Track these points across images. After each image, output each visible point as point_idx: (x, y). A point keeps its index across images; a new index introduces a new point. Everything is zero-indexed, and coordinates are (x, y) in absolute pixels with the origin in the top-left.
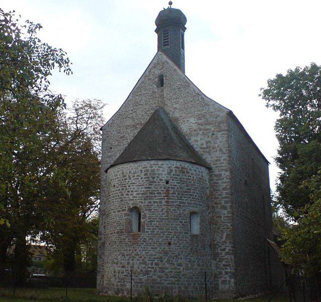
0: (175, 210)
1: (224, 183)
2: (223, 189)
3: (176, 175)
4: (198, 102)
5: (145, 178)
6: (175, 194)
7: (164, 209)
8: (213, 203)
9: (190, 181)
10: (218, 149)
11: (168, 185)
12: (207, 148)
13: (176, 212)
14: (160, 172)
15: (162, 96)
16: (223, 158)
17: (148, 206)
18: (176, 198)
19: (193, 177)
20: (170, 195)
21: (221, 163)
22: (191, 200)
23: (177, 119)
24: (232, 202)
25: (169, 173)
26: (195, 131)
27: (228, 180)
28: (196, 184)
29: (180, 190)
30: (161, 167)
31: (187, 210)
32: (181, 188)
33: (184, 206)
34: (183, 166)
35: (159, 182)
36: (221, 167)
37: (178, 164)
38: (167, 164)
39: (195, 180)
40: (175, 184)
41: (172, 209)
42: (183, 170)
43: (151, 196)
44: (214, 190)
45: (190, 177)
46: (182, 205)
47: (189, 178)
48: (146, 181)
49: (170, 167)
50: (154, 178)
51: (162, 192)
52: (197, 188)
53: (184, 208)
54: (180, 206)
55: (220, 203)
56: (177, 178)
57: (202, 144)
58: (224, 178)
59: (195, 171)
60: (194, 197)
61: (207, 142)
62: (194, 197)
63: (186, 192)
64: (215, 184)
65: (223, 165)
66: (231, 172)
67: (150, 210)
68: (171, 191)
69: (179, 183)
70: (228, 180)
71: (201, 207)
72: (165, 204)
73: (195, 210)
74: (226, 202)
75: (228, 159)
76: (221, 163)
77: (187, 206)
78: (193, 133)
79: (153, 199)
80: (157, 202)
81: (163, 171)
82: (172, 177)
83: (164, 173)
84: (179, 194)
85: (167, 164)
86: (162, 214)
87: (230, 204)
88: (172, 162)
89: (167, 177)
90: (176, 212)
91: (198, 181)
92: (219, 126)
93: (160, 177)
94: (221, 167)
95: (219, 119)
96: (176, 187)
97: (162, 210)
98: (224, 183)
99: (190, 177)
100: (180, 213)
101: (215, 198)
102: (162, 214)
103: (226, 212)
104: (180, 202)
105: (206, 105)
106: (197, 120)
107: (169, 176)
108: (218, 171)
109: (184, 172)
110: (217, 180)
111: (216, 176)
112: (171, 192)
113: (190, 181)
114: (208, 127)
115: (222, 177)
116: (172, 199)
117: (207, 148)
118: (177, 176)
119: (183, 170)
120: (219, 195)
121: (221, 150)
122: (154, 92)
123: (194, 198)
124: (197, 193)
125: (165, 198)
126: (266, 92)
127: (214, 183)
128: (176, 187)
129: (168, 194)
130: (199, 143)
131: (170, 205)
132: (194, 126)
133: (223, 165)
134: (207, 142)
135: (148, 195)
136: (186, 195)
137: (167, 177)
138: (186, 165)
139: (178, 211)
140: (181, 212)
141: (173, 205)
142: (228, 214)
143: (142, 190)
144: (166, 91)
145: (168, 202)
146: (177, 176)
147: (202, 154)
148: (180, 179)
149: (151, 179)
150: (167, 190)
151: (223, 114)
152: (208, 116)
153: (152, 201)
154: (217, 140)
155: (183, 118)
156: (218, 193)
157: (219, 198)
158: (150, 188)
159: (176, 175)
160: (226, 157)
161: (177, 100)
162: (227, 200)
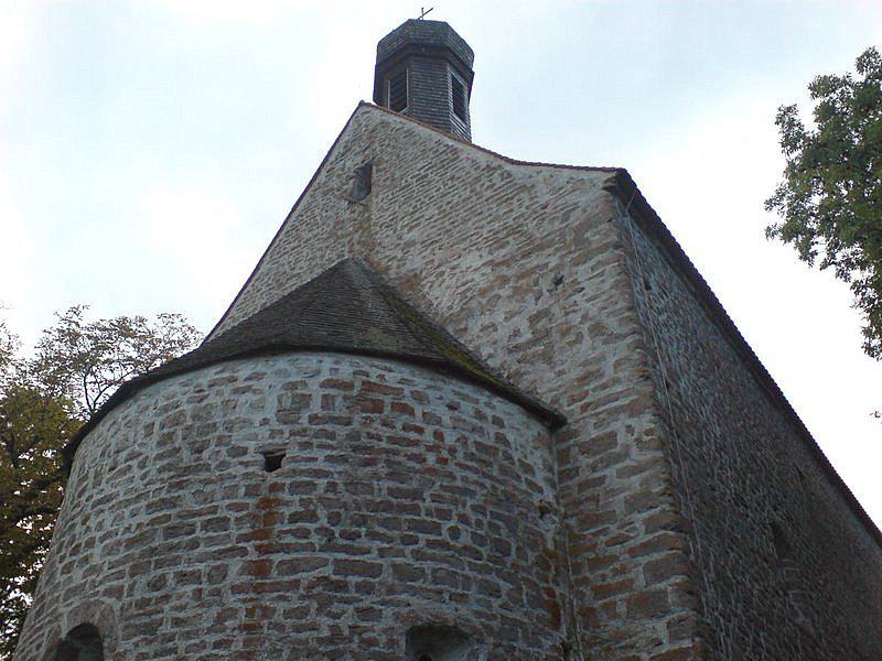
0: (304, 612)
1: (634, 471)
2: (633, 505)
3: (325, 420)
4: (489, 193)
5: (160, 457)
6: (313, 517)
7: (233, 613)
8: (587, 590)
9: (414, 450)
10: (585, 328)
11: (272, 477)
12: (534, 342)
13: (314, 627)
14: (242, 412)
15: (364, 225)
16: (612, 361)
17: (146, 602)
18: (315, 539)
19: (438, 436)
20: (278, 527)
21: (604, 387)
22: (419, 556)
23: (413, 280)
24: (693, 571)
25: (286, 415)
26: (483, 292)
27: (649, 455)
28: (459, 473)
29: (347, 497)
30: (244, 391)
31: (388, 611)
32: (352, 485)
33: (366, 589)
34: (373, 379)
35: (223, 465)
36: (609, 400)
37: (346, 368)
38: (279, 373)
39: (452, 451)
40: (321, 465)
41: (281, 606)
42: (372, 396)
43: (171, 548)
44: (588, 521)
45: (420, 430)
46: (353, 579)
47: (413, 436)
48: (160, 471)
49: (293, 386)
50: (200, 451)
51: (232, 515)
52: (465, 492)
53: (367, 602)
54: (342, 586)
55: (623, 586)
56: (332, 436)
57: (516, 333)
58: (628, 447)
59: (452, 407)
60: (445, 536)
61: (534, 320)
62: (445, 536)
63: (388, 507)
64: (588, 493)
65: (619, 388)
66: (662, 415)
67: (150, 629)
68: (292, 503)
69: (343, 459)
70: (649, 455)
71: (496, 602)
72: (246, 578)
73: (449, 612)
74: (657, 573)
75: (636, 356)
76: (604, 387)
77: (391, 591)
78: (474, 304)
79: (175, 561)
80: (195, 577)
81: (257, 407)
82: (303, 432)
83: (257, 418)
84: (334, 519)
85: (279, 373)
86: (217, 645)
87: (678, 579)
88: (310, 361)
89: (273, 434)
90: (314, 627)
91: (471, 457)
92: (580, 241)
93: (237, 438)
94: (609, 400)
95: (576, 218)
96: (322, 482)
97: (220, 619)
98: (634, 471)
99: (420, 430)
100: (336, 631)
101: (596, 563)
102: (217, 645)
103: (660, 628)
104: (341, 567)
105: (523, 188)
106: (490, 253)
107: (286, 429)
108: (596, 426)
109: (377, 407)
110: (594, 468)
111: (586, 449)
112: (287, 511)
113: (414, 450)
114: (534, 261)
115: (618, 449)
116: (287, 548)
117: (534, 342)
118: (329, 427)
119: (369, 399)
120: (615, 541)
121: (597, 329)
122: (339, 224)
123: (444, 545)
124: (464, 519)
125: (250, 546)
126: (801, 258)
127: (582, 486)
128: (322, 482)
129: (270, 518)
130: (502, 333)
131: (276, 587)
132: (477, 276)
133: (619, 388)
134: (534, 320)
135: (158, 542)
136: (385, 523)
137: (273, 434)
138: (395, 375)
139: (325, 621)
140: (344, 623)
141: (295, 584)
142: (674, 637)
143: (134, 522)
144: (377, 200)
145: (260, 569)
146: (329, 427)
147: (519, 374)
148: (350, 437)
149: (187, 457)
150: (266, 503)
151: (592, 198)
152: (531, 226)
153: (170, 572)
154: (577, 297)
155: (439, 266)
156: (604, 532)
157: (614, 558)
158: (173, 503)
159: (325, 420)
160: (625, 353)
161: (417, 215)
162: (656, 556)
